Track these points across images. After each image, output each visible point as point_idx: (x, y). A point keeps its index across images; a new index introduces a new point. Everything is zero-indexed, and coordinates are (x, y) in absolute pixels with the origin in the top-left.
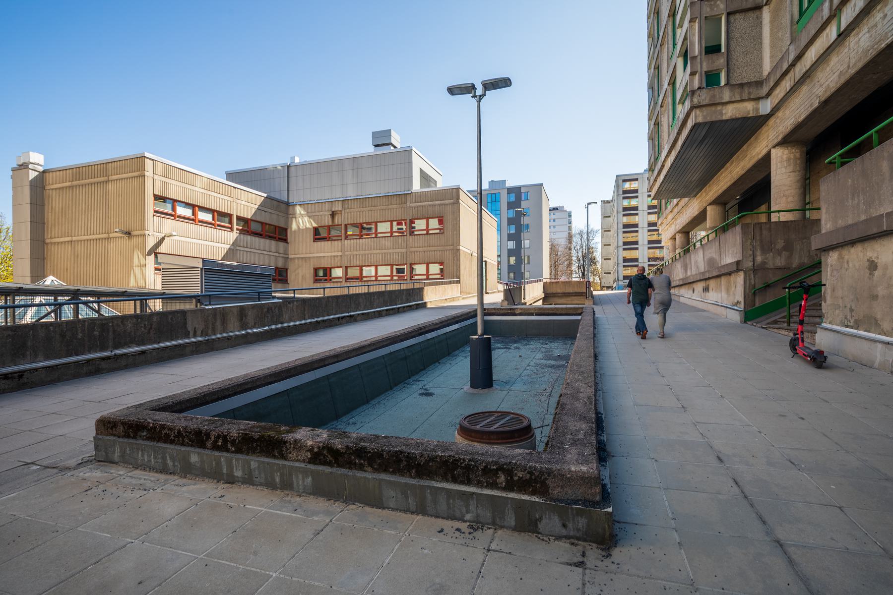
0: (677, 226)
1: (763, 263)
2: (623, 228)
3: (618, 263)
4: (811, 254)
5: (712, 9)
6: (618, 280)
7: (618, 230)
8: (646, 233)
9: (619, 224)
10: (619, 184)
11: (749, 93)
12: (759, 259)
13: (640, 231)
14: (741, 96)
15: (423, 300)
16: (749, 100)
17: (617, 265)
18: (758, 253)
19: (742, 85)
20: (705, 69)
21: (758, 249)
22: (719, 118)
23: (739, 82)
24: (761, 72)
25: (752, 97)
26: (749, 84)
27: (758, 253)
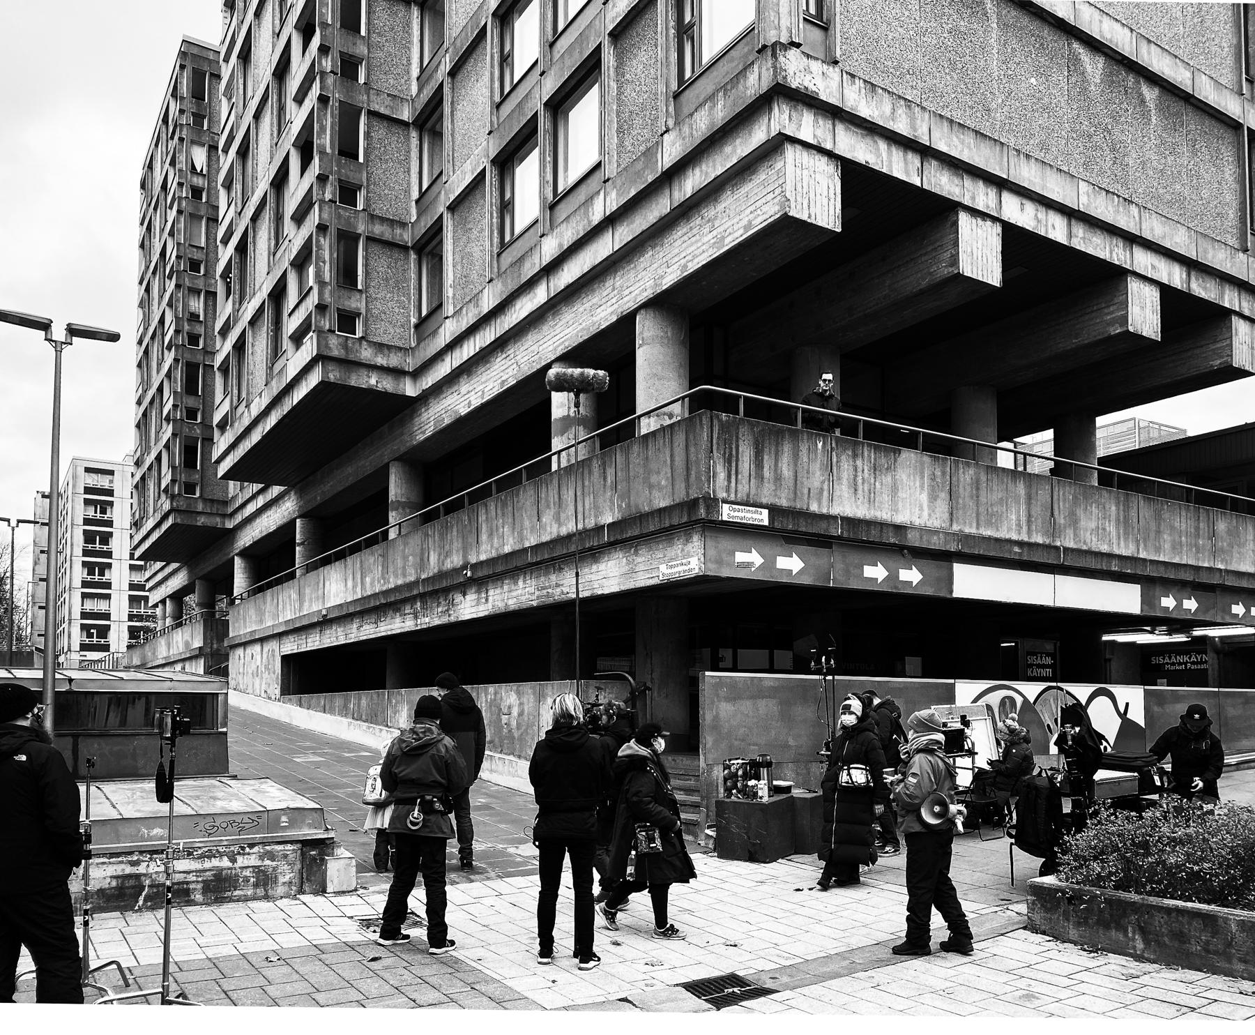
0: (168, 589)
1: (218, 650)
2: (83, 556)
3: (70, 620)
4: (1151, 436)
5: (190, 431)
6: (69, 650)
7: (73, 558)
8: (117, 488)
9: (75, 547)
10: (78, 473)
11: (218, 509)
12: (215, 646)
13: (115, 564)
14: (211, 510)
15: (286, 659)
16: (217, 514)
17: (70, 623)
18: (215, 642)
19: (212, 501)
20: (183, 479)
21: (215, 638)
22: (194, 523)
23: (210, 497)
24: (227, 493)
25: (219, 512)
26: (218, 501)
27: (215, 642)
